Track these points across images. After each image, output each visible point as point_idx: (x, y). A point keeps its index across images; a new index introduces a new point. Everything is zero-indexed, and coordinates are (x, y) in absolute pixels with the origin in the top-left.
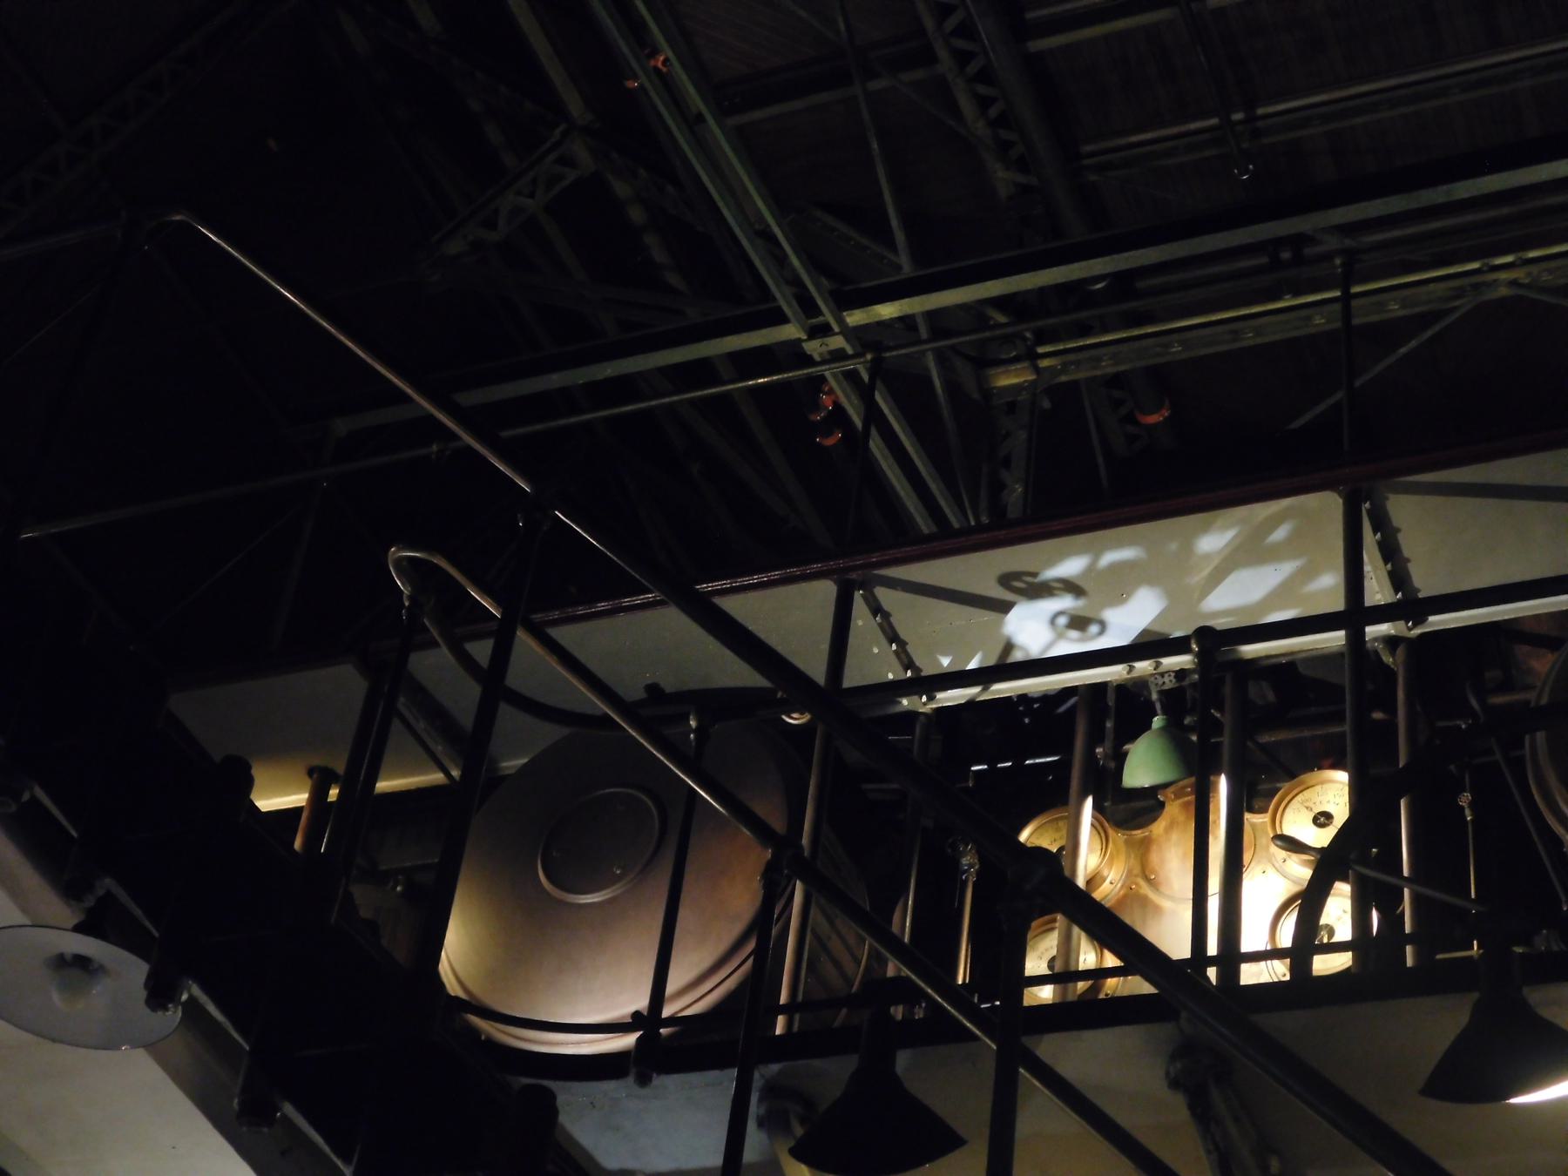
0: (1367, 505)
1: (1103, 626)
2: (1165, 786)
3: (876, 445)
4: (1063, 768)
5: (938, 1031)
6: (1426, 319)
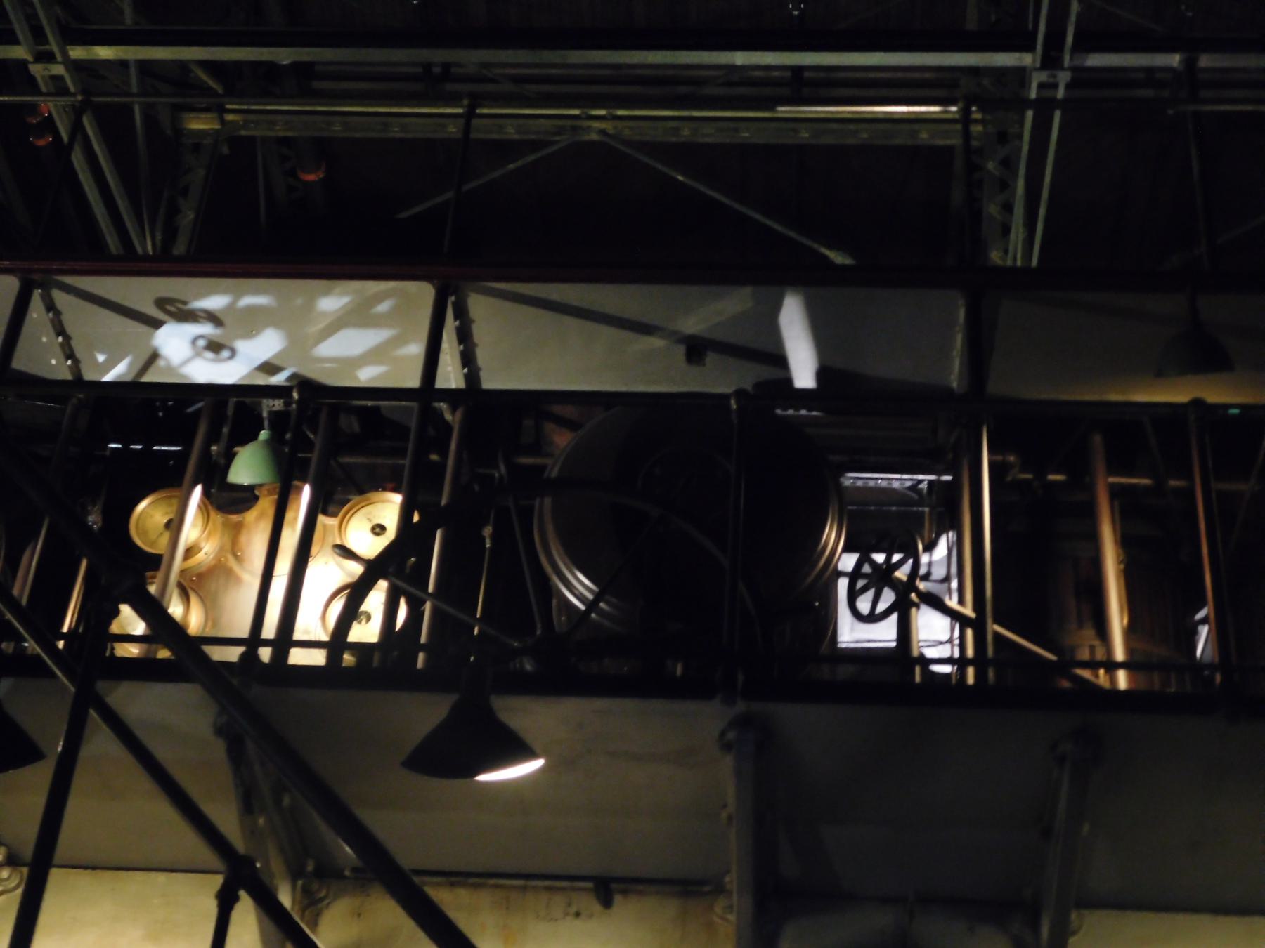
0: (453, 298)
1: (233, 353)
2: (261, 485)
4: (182, 458)
6: (535, 145)
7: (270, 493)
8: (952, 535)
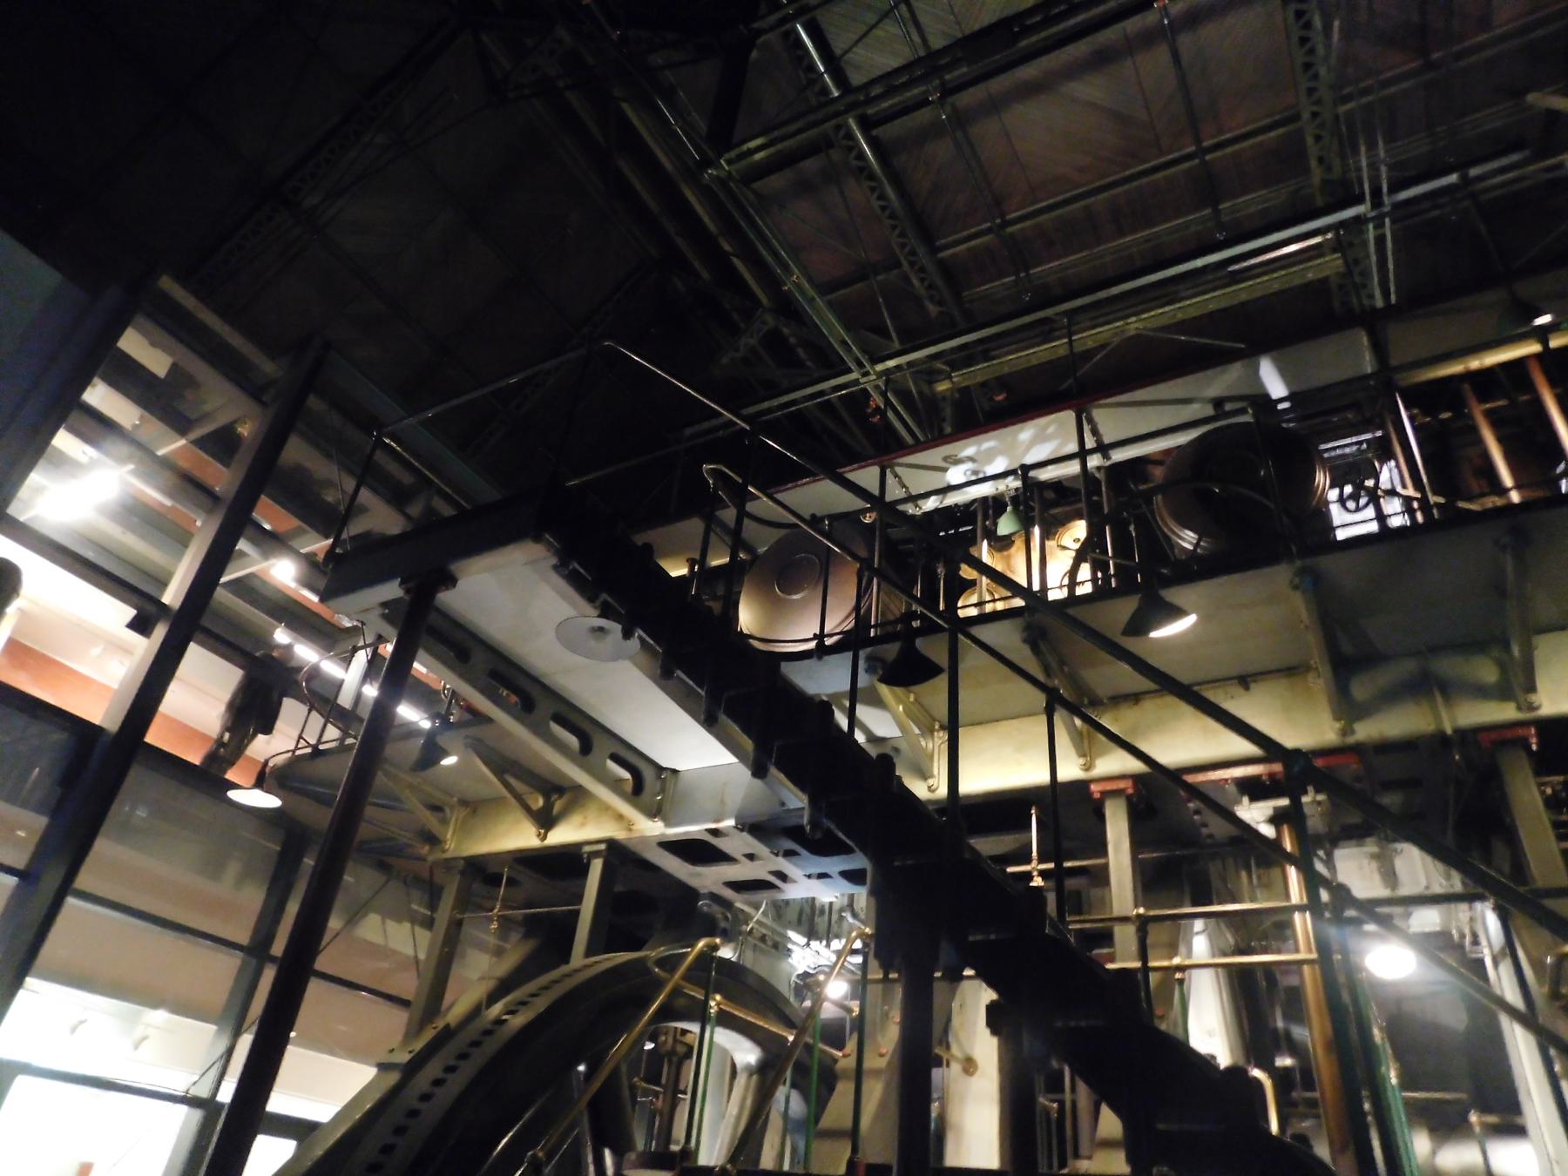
3: (890, 414)
4: (974, 531)
5: (930, 629)
6: (1103, 347)
7: (1020, 537)
8: (1393, 463)
